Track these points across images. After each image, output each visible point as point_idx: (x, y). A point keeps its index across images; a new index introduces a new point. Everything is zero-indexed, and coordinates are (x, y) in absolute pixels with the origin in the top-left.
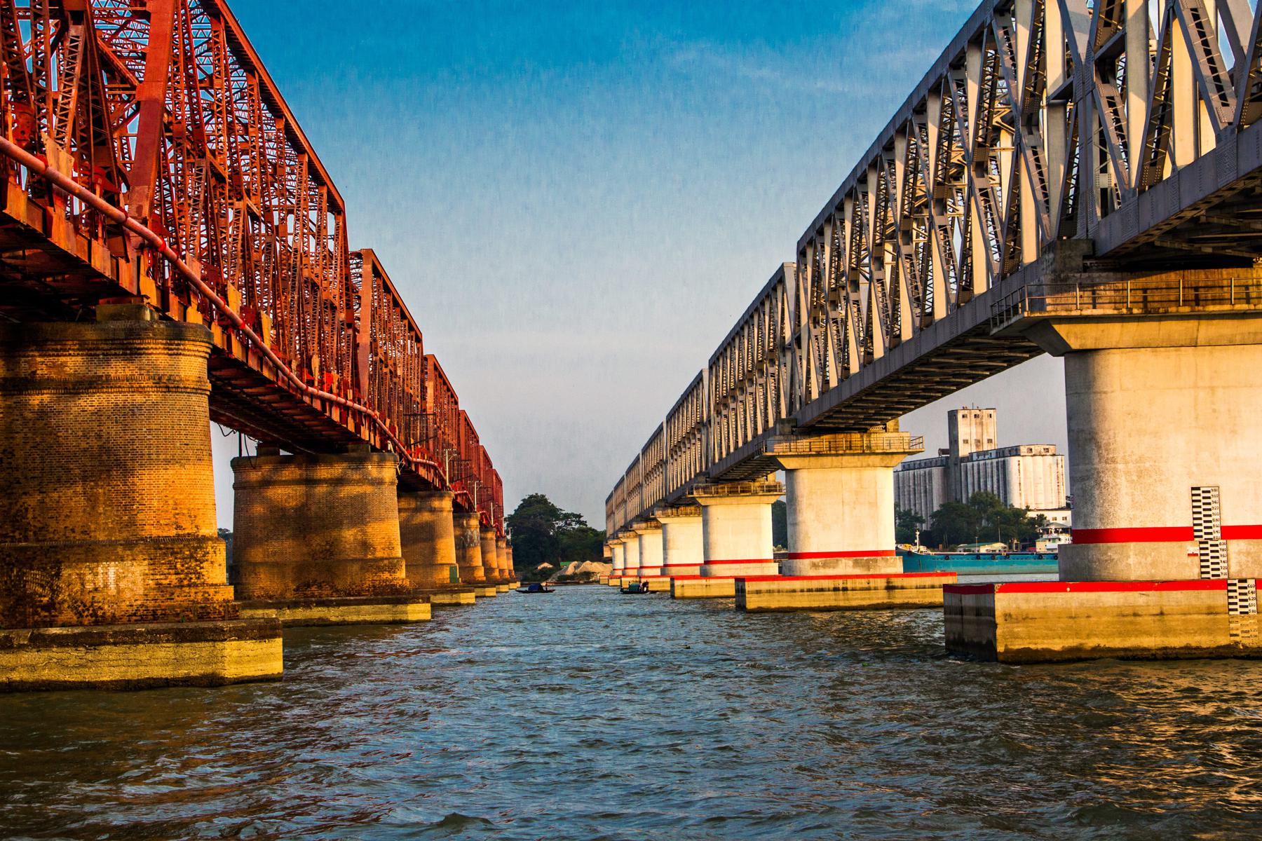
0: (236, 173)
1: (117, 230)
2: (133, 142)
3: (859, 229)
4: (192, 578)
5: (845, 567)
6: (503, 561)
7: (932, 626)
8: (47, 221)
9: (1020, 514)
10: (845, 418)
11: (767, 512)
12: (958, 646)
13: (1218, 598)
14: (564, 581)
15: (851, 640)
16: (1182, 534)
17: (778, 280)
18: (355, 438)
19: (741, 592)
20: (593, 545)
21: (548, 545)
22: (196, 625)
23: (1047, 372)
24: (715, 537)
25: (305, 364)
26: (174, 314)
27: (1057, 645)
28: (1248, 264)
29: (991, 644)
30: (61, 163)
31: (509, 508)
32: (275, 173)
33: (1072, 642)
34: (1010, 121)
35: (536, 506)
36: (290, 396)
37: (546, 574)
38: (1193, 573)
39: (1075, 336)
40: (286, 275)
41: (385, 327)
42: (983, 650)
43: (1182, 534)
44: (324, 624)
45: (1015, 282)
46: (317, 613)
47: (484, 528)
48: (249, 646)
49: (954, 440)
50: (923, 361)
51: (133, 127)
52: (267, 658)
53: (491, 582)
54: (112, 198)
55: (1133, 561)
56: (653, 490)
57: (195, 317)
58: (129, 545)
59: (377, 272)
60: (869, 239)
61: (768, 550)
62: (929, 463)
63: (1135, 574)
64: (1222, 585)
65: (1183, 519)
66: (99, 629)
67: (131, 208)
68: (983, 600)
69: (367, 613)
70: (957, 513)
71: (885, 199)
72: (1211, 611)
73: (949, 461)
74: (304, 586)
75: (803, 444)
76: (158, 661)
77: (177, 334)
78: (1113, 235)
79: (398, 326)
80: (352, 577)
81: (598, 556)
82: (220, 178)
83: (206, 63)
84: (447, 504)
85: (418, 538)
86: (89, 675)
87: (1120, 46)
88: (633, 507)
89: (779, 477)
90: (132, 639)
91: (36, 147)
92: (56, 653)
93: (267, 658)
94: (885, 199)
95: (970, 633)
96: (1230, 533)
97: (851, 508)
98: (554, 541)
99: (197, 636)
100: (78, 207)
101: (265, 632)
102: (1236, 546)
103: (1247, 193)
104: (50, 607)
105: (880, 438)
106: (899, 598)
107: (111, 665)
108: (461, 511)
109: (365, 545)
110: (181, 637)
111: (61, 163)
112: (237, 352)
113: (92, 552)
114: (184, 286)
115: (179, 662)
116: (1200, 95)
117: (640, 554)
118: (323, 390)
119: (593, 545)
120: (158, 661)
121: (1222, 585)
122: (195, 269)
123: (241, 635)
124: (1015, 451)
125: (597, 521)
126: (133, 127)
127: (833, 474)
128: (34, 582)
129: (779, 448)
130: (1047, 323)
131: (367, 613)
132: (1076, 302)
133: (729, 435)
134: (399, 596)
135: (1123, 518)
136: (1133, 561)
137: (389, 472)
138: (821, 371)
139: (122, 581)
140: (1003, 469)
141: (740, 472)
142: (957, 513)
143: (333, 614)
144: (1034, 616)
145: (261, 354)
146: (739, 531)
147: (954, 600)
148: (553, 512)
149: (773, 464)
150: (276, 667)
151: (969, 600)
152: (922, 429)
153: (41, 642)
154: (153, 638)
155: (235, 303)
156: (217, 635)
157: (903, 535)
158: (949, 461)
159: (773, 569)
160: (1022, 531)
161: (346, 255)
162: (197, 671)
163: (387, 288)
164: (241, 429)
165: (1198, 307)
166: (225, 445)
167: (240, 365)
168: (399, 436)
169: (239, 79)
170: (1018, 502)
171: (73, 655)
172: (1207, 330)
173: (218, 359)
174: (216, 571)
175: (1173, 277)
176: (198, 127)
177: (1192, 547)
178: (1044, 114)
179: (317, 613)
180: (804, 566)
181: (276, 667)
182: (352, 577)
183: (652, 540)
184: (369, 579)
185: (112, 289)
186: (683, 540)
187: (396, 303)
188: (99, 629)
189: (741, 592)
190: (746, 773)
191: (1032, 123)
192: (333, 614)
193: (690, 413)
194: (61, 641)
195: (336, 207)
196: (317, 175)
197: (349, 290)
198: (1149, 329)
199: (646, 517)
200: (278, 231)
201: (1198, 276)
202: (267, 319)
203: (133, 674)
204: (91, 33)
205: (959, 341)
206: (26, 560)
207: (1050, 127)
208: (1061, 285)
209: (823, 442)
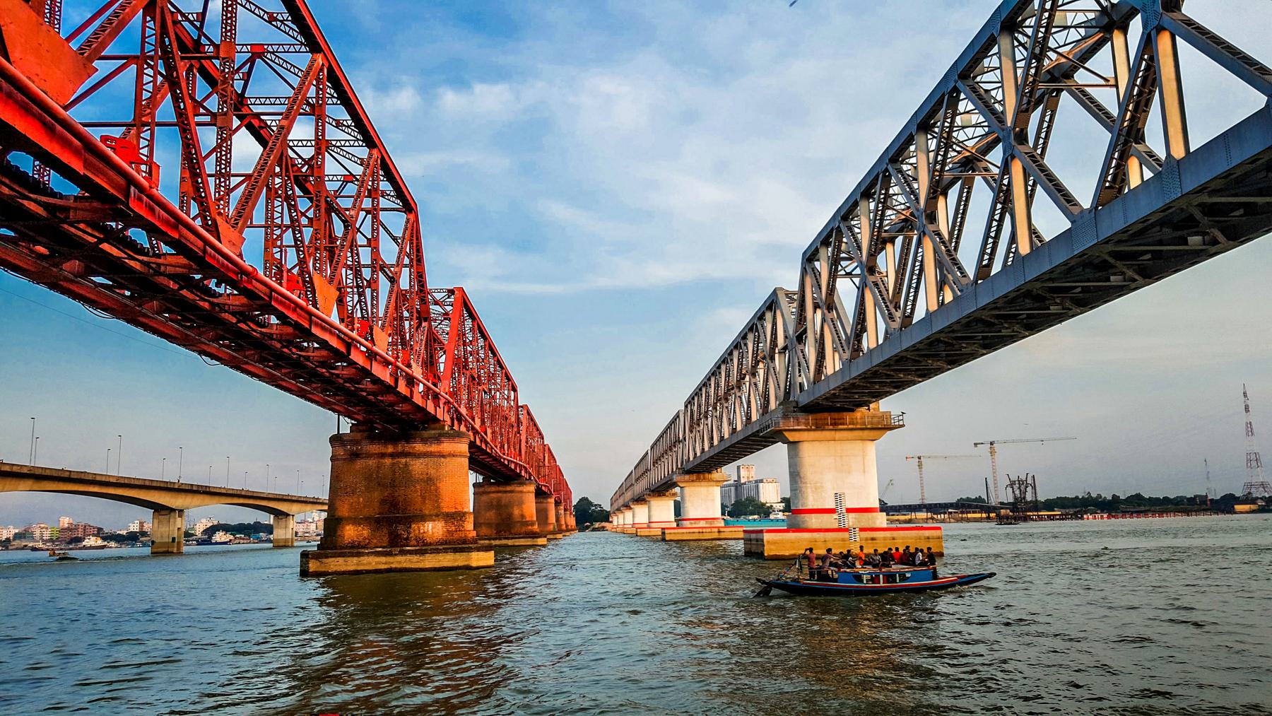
0: (479, 376)
1: (436, 397)
2: (442, 366)
3: (708, 396)
4: (460, 528)
5: (702, 524)
6: (572, 521)
7: (740, 546)
8: (412, 392)
9: (763, 504)
10: (702, 469)
11: (672, 504)
12: (748, 554)
13: (846, 535)
14: (594, 530)
15: (706, 550)
16: (832, 511)
17: (677, 416)
18: (519, 476)
19: (663, 533)
20: (605, 517)
21: (589, 517)
22: (461, 546)
23: (780, 449)
24: (653, 513)
25: (502, 447)
26: (455, 427)
27: (787, 553)
28: (853, 411)
29: (762, 553)
30: (417, 371)
31: (574, 503)
32: (491, 377)
33: (793, 552)
34: (764, 358)
35: (584, 501)
36: (497, 459)
37: (587, 527)
38: (836, 526)
39: (791, 437)
40: (496, 414)
41: (531, 434)
42: (760, 555)
43: (832, 511)
44: (507, 546)
45: (767, 417)
46: (504, 542)
47: (565, 510)
48: (481, 554)
49: (739, 477)
50: (733, 446)
51: (443, 359)
52: (487, 558)
53: (568, 530)
54: (435, 385)
55: (814, 521)
56: (628, 495)
57: (463, 428)
58: (437, 515)
59: (529, 413)
60: (712, 401)
61: (672, 518)
62: (730, 486)
63: (815, 526)
64: (846, 530)
65: (831, 505)
66: (425, 547)
67: (443, 389)
68: (759, 536)
69: (522, 542)
70: (742, 505)
71: (717, 385)
72: (843, 540)
73: (738, 485)
74: (498, 532)
75: (687, 477)
76: (447, 560)
77: (457, 436)
78: (804, 400)
79: (535, 433)
80: (517, 529)
81: (607, 520)
82: (473, 378)
83: (470, 337)
84: (552, 500)
85: (542, 514)
86: (421, 565)
87: (805, 331)
88: (621, 502)
89: (677, 490)
90: (437, 551)
91: (409, 366)
92: (409, 557)
93: (487, 558)
94: (717, 385)
95: (754, 549)
96: (849, 510)
97: (704, 502)
98: (591, 515)
99: (462, 550)
100: (421, 387)
101: (487, 549)
102: (852, 515)
103: (853, 384)
104: (407, 539)
105: (716, 475)
106: (723, 536)
107: (430, 561)
108: (557, 503)
109: (522, 516)
110: (455, 551)
111: (417, 371)
112: (478, 442)
113: (423, 518)
114: (460, 418)
115: (455, 560)
116: (835, 350)
117: (624, 520)
118: (509, 457)
119: (605, 517)
120: (447, 560)
121: (846, 530)
122: (463, 411)
123: (479, 549)
124: (761, 481)
125: (607, 507)
126: (443, 359)
127: (697, 489)
128: (401, 530)
129: (675, 478)
130: (780, 432)
131: (522, 542)
132: (792, 424)
133: (657, 475)
134: (534, 535)
135: (811, 505)
136: (814, 521)
137: (532, 488)
138: (695, 449)
139: (433, 529)
140: (757, 487)
141: (662, 489)
142: (742, 505)
143: (510, 542)
144: (778, 542)
145: (487, 443)
146: (662, 511)
147: (747, 536)
148: (591, 504)
149: (675, 485)
150: (492, 562)
151: (753, 536)
152: (728, 472)
153: (403, 553)
154: (445, 551)
155: (477, 425)
156: (470, 550)
157: (723, 514)
158: (738, 485)
159: (674, 525)
160: (765, 511)
161: (518, 407)
162: (461, 564)
163: (532, 419)
164: (476, 472)
165: (835, 425)
166: (473, 478)
167: (479, 448)
168: (534, 474)
169: (481, 342)
170: (763, 500)
171: (415, 558)
172: (838, 435)
173: (472, 445)
174: (469, 525)
175: (826, 415)
176: (466, 360)
177: (835, 516)
178: (777, 356)
179: (504, 542)
180: (687, 524)
181: (492, 562)
182: (517, 529)
183: (628, 514)
184: (523, 530)
185: (435, 420)
186: (640, 515)
187: (535, 425)
188: (425, 547)
189: (663, 533)
190: (1183, 612)
191: (772, 359)
192: (510, 542)
193: (642, 469)
194: (410, 552)
195: (514, 389)
196: (508, 378)
197: (519, 421)
198: (818, 434)
199: (627, 506)
200: (494, 397)
201: (835, 415)
202: (489, 431)
203: (437, 565)
204: (430, 325)
205: (746, 439)
206: (399, 521)
207: (779, 362)
208: (785, 417)
209: (694, 476)
